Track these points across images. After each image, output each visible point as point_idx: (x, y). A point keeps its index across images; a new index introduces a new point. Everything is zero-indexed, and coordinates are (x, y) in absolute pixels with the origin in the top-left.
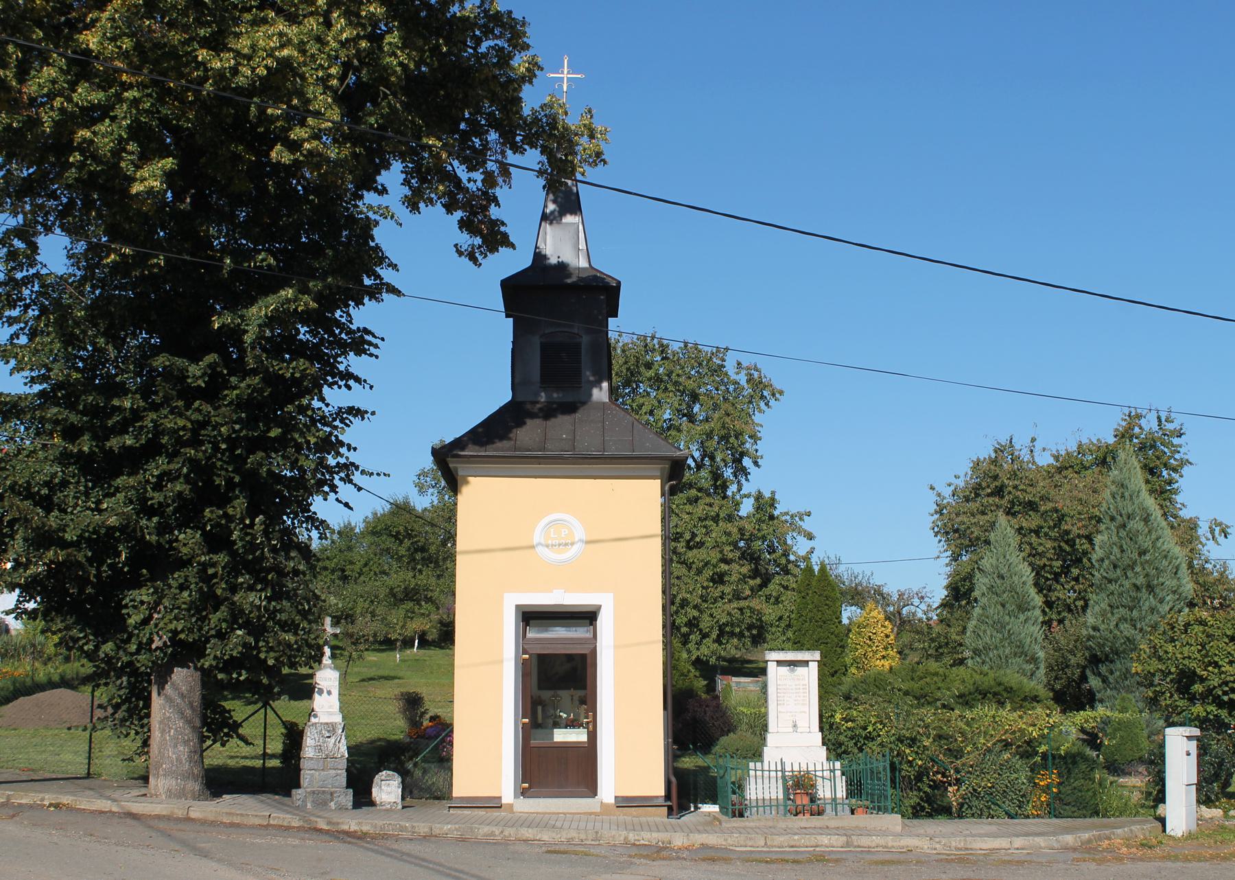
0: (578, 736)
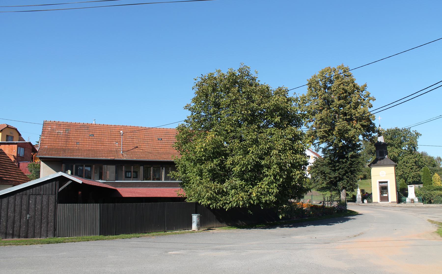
0: (386, 195)
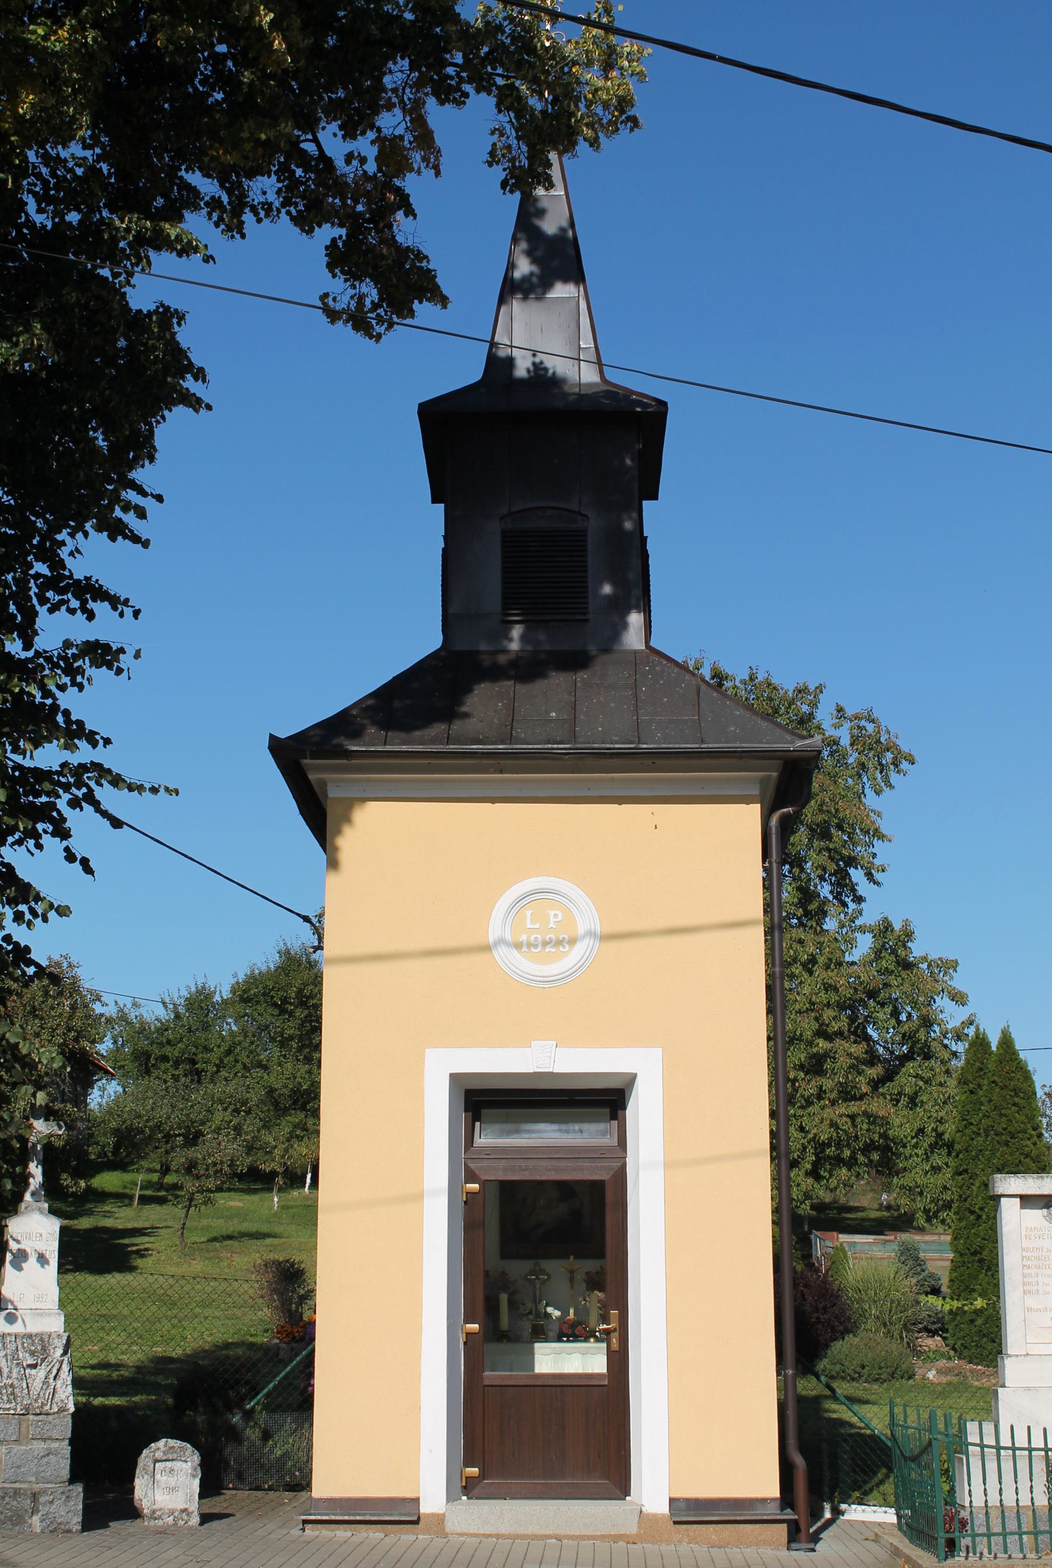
0: (586, 1360)
